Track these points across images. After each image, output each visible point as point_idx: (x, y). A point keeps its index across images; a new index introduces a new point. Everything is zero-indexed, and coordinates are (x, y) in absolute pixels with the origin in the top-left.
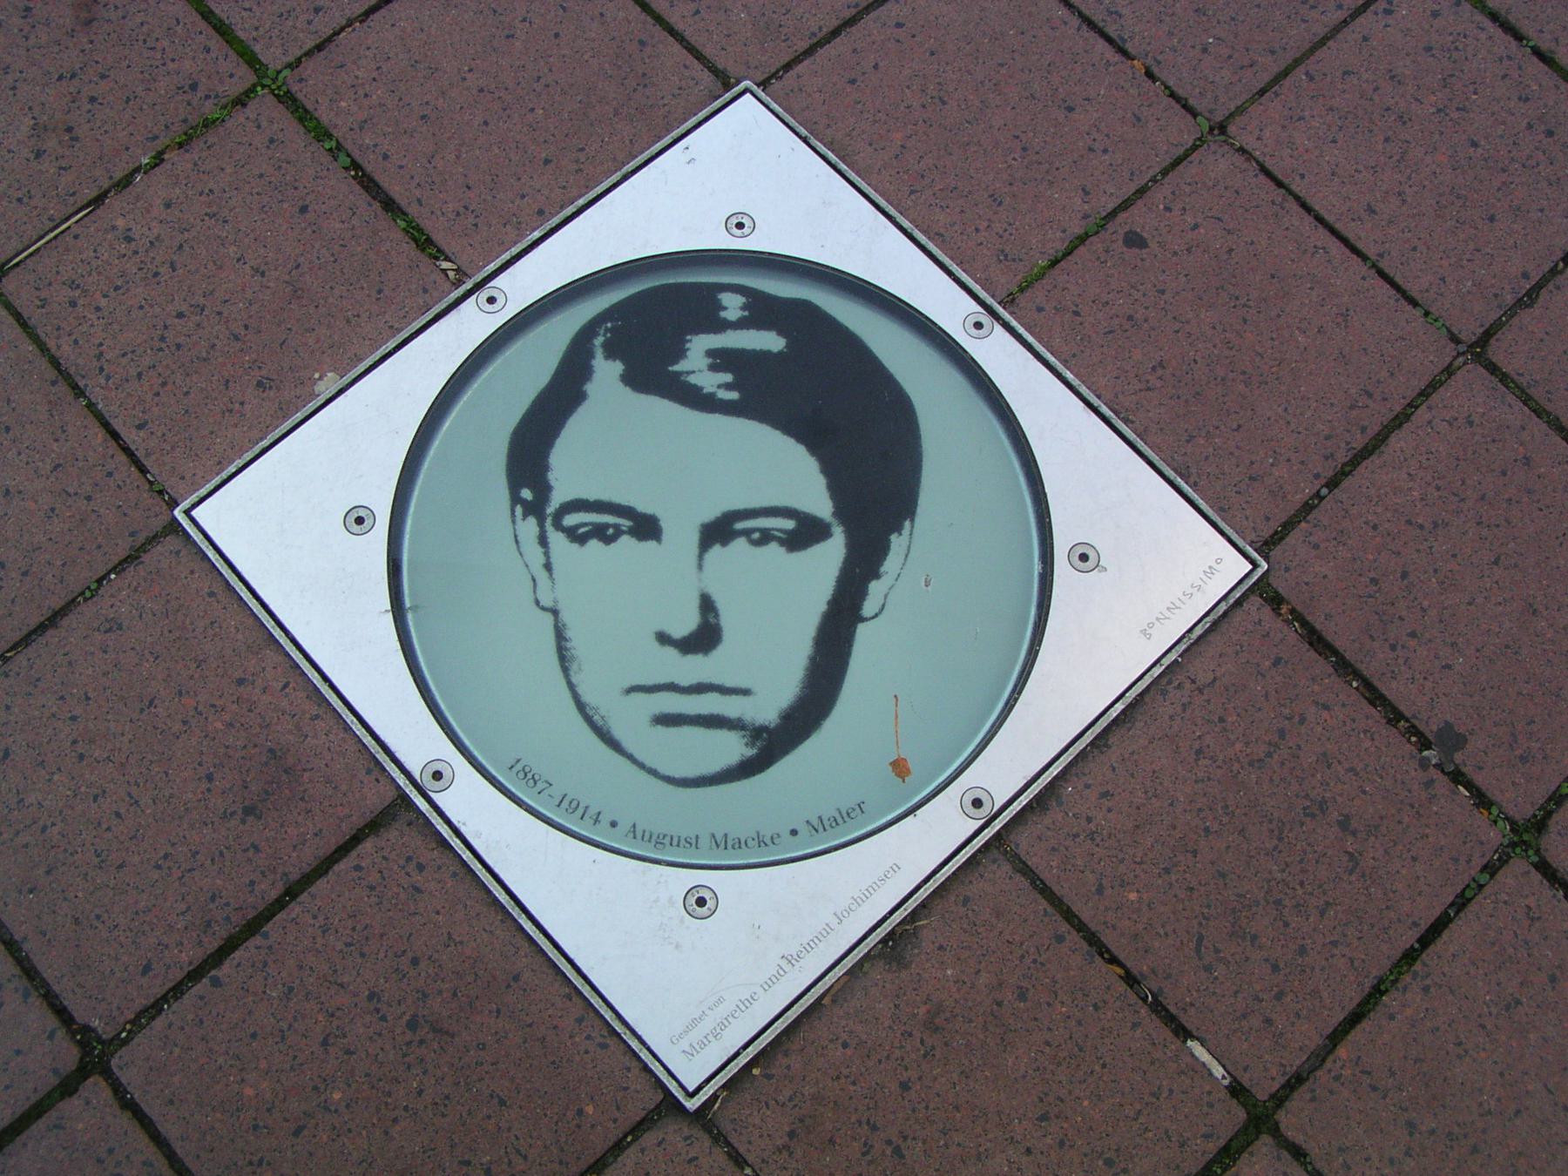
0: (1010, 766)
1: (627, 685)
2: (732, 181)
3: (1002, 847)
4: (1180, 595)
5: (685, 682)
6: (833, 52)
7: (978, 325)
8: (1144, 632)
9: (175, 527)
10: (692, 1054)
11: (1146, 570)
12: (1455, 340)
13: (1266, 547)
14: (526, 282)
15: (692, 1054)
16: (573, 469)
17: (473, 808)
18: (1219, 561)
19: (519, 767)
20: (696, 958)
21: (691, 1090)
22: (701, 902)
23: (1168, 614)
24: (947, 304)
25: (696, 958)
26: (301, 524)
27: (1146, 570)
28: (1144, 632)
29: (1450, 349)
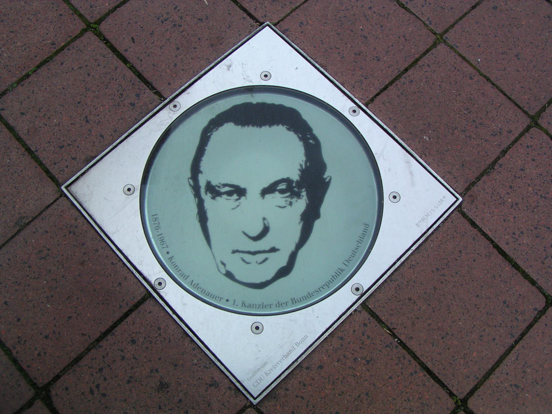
0: (368, 276)
1: (249, 265)
2: (266, 59)
3: (368, 308)
4: (430, 210)
5: (252, 250)
6: (487, 162)
7: (354, 111)
8: (417, 224)
9: (63, 194)
11: (415, 200)
12: (435, 34)
13: (260, 25)
14: (187, 100)
16: (213, 172)
17: (174, 295)
18: (444, 197)
20: (254, 347)
21: (255, 396)
22: (257, 328)
24: (342, 103)
25: (254, 347)
26: (112, 195)
27: (415, 200)
28: (417, 224)
29: (434, 37)
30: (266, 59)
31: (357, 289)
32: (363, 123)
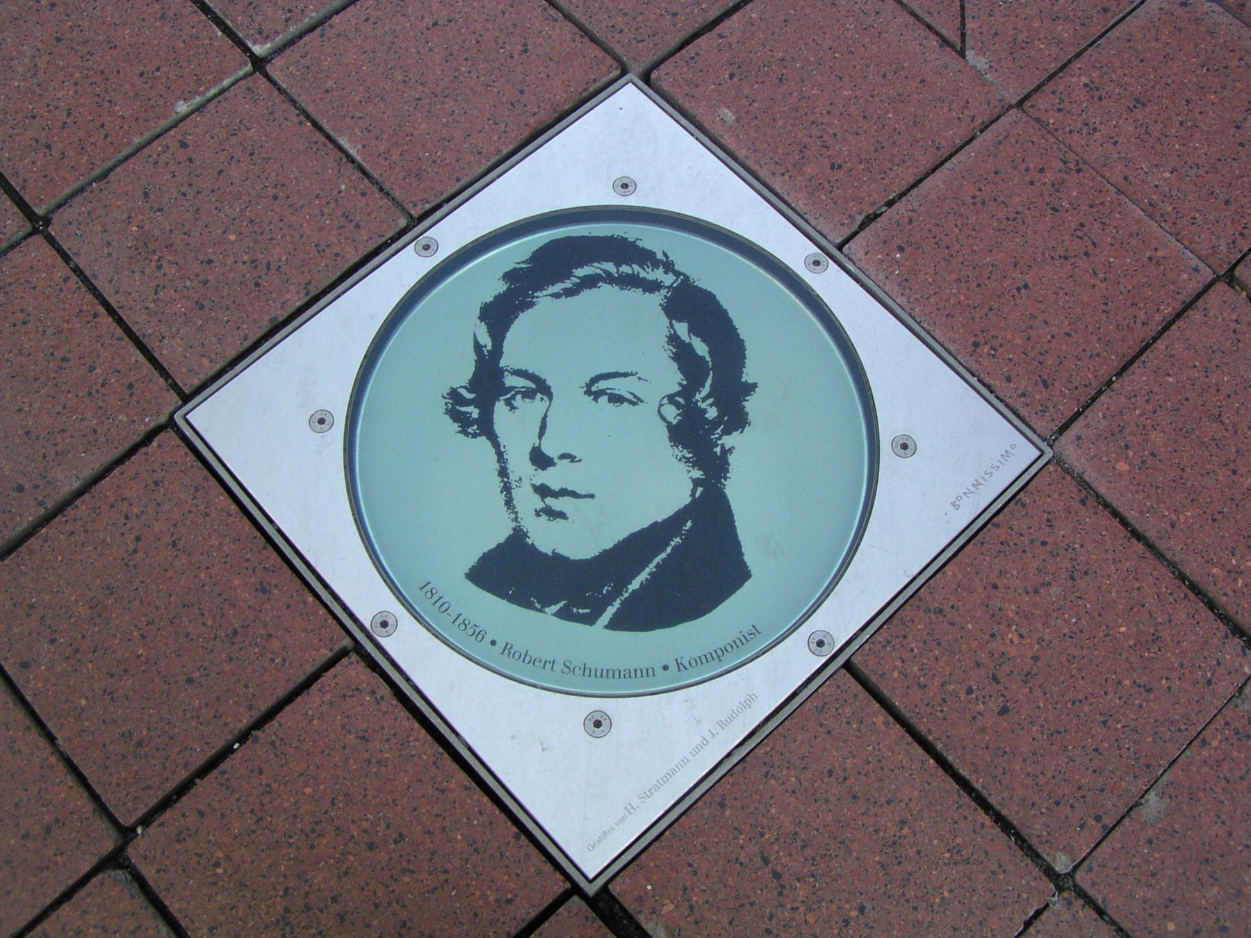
7: (817, 263)
8: (953, 504)
10: (213, 419)
15: (213, 419)
18: (1013, 446)
19: (460, 620)
23: (973, 489)
25: (595, 759)
26: (275, 427)
27: (949, 451)
30: (626, 151)
31: (427, 247)
32: (834, 285)
